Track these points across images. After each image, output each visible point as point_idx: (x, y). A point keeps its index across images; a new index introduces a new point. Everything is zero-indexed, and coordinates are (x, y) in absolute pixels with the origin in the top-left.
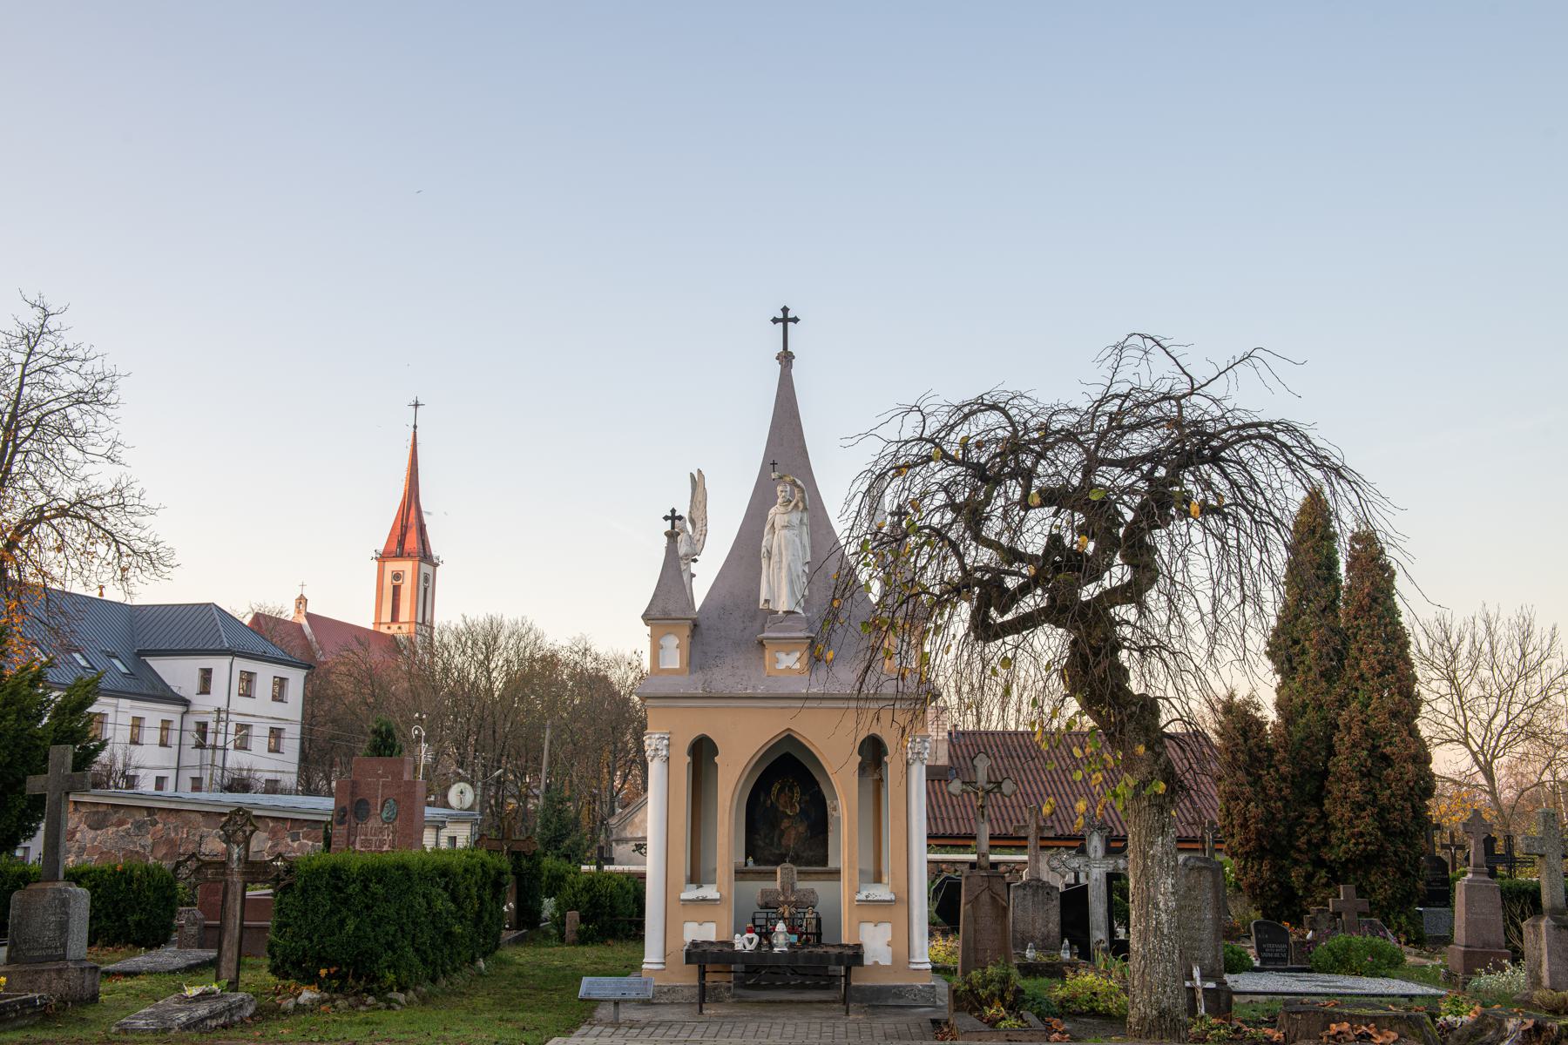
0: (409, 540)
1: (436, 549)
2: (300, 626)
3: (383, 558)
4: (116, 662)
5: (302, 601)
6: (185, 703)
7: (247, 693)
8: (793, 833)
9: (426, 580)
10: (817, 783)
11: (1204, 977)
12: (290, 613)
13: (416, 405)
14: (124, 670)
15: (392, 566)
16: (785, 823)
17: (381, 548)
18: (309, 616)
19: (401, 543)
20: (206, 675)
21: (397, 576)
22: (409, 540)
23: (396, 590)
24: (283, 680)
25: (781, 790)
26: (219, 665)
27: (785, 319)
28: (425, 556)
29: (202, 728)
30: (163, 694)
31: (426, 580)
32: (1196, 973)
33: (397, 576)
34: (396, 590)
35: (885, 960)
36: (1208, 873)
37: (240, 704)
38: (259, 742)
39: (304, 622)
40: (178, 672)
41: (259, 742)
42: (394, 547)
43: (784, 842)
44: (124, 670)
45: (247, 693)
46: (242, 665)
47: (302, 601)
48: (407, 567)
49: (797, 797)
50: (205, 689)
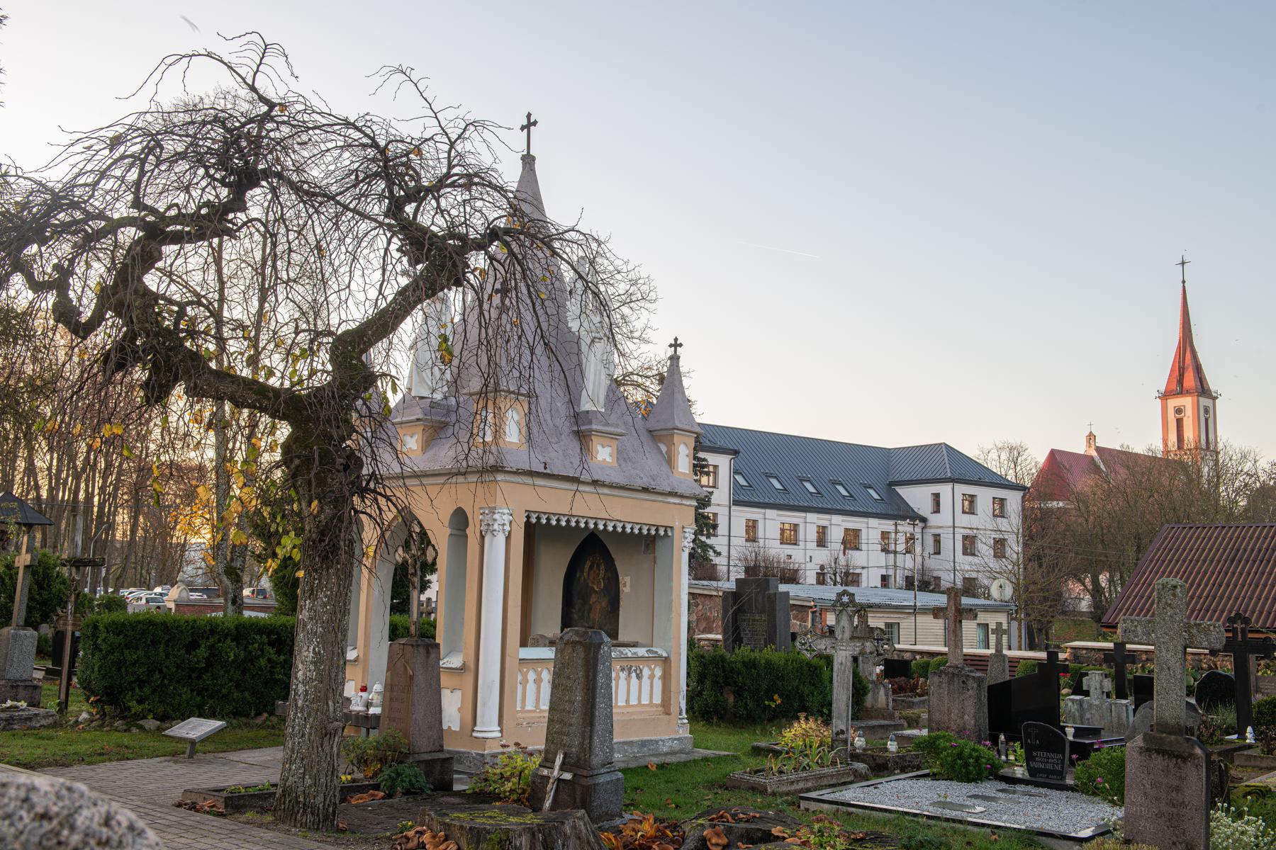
0: (1188, 378)
1: (1213, 385)
2: (1092, 457)
3: (1165, 396)
4: (872, 492)
5: (1091, 437)
6: (924, 520)
7: (972, 511)
8: (599, 604)
9: (1206, 411)
10: (613, 560)
11: (563, 768)
12: (1080, 448)
13: (1183, 263)
14: (876, 497)
15: (1173, 403)
16: (593, 599)
17: (1163, 389)
18: (1098, 449)
19: (1181, 381)
20: (937, 497)
21: (1179, 410)
22: (1188, 378)
23: (1179, 423)
24: (972, 496)
25: (591, 567)
26: (945, 490)
27: (529, 125)
28: (1203, 390)
29: (937, 539)
30: (905, 513)
31: (1206, 411)
32: (559, 760)
33: (1179, 410)
34: (1179, 423)
35: (456, 727)
36: (580, 649)
37: (964, 520)
38: (985, 549)
39: (1094, 454)
40: (918, 497)
41: (985, 549)
42: (1174, 386)
43: (592, 616)
44: (876, 497)
45: (972, 511)
46: (962, 489)
47: (1091, 437)
48: (1187, 402)
49: (602, 572)
50: (937, 510)
